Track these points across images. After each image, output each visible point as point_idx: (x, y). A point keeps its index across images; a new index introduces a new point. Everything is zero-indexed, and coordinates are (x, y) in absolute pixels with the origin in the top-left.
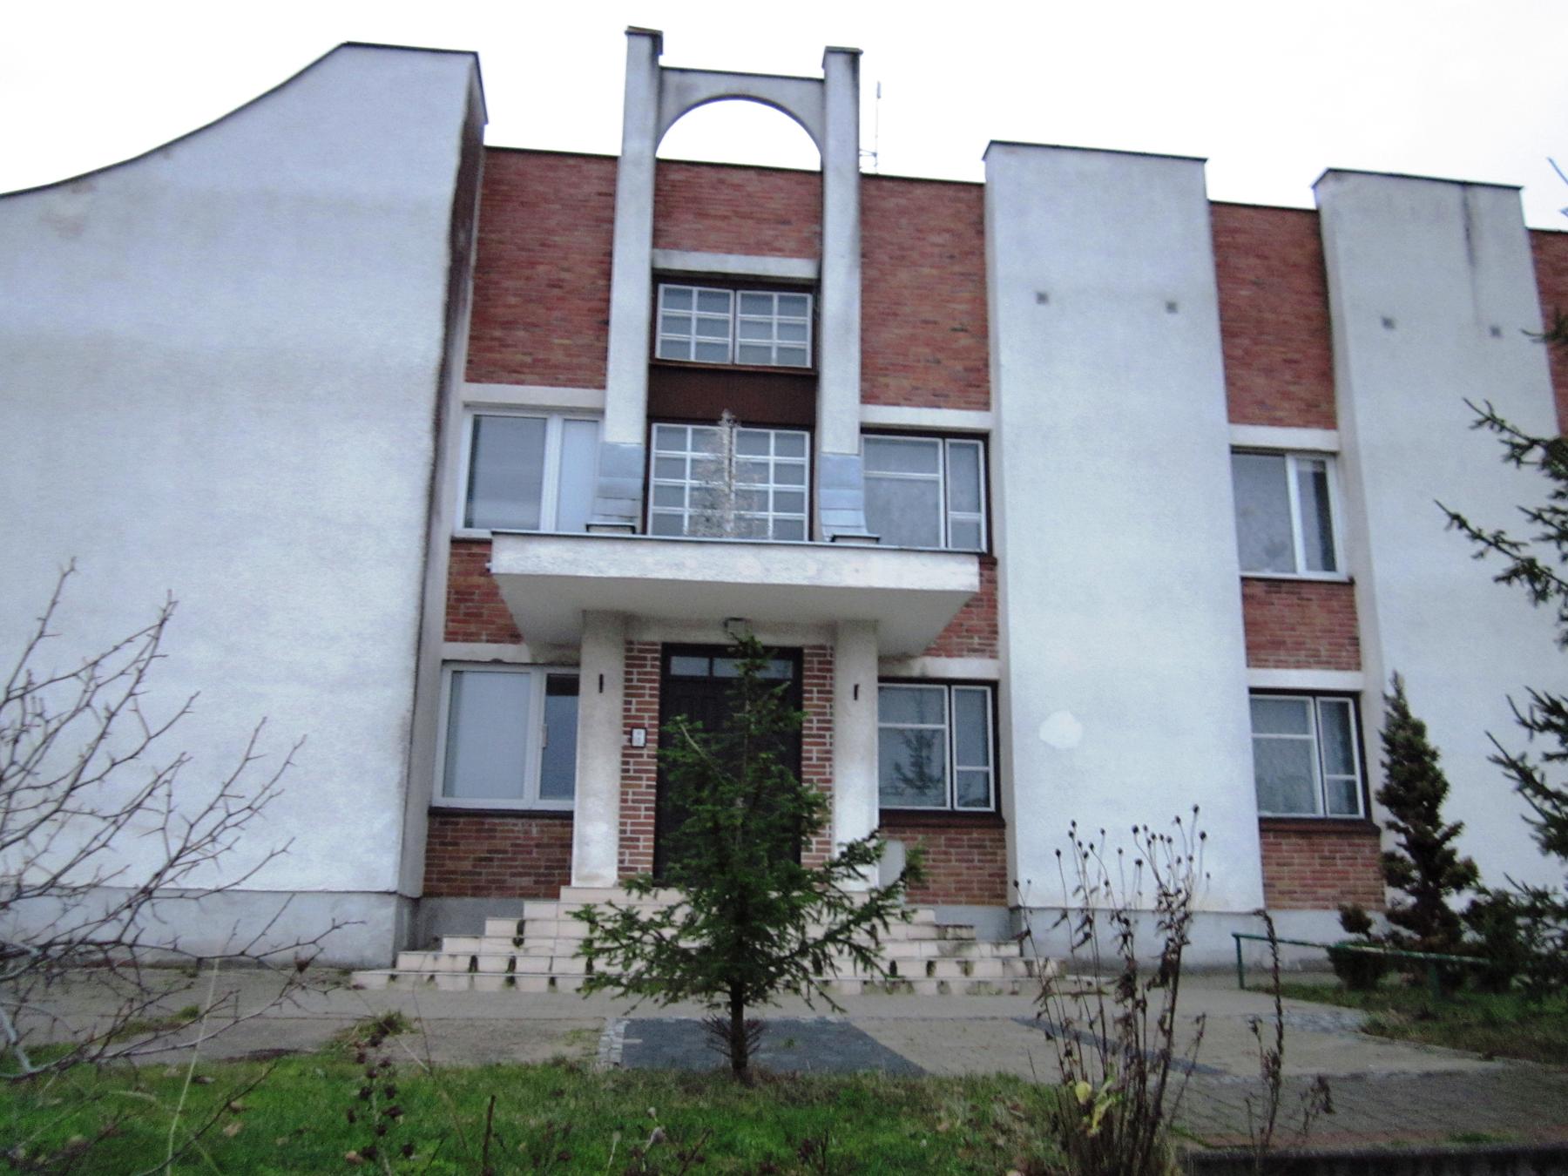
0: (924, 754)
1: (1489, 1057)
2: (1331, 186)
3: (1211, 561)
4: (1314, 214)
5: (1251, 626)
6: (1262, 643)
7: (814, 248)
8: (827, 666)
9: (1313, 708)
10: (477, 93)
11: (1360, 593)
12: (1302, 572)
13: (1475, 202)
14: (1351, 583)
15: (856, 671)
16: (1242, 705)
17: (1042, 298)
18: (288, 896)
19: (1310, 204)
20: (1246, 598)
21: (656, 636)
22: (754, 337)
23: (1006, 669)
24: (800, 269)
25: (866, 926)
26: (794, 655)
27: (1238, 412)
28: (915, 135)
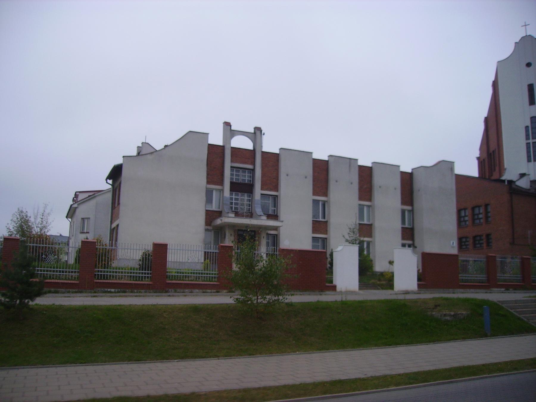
0: (271, 248)
2: (330, 157)
3: (309, 218)
4: (327, 161)
5: (313, 227)
6: (314, 231)
7: (254, 163)
8: (259, 234)
9: (320, 240)
10: (493, 146)
11: (328, 223)
12: (321, 219)
13: (352, 161)
14: (327, 222)
15: (264, 235)
16: (310, 240)
17: (287, 175)
18: (154, 150)
19: (278, 153)
20: (313, 223)
21: (237, 228)
22: (245, 178)
23: (279, 233)
24: (251, 167)
26: (254, 231)
27: (314, 194)
28: (270, 145)
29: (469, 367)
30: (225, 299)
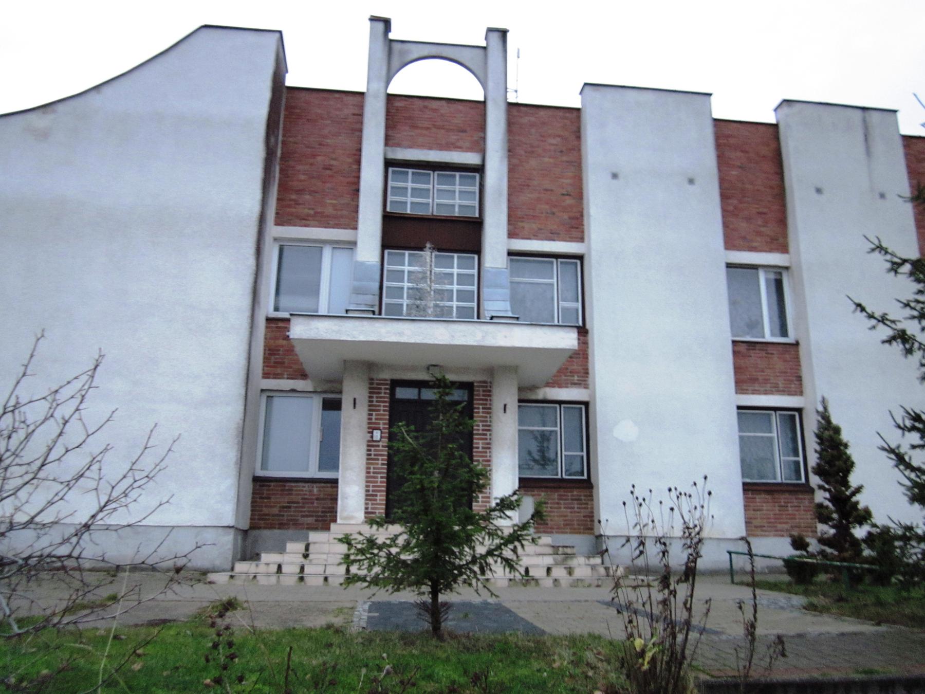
0: (545, 445)
2: (785, 109)
3: (715, 331)
4: (775, 127)
5: (738, 369)
6: (744, 379)
7: (480, 146)
8: (488, 393)
9: (775, 418)
11: (802, 350)
12: (768, 338)
13: (870, 119)
14: (797, 344)
15: (505, 396)
16: (732, 416)
17: (615, 176)
20: (735, 353)
21: (387, 375)
22: (445, 199)
23: (593, 395)
24: (472, 158)
26: (468, 387)
27: (730, 243)
28: (540, 80)
29: (428, 162)
30: (658, 670)
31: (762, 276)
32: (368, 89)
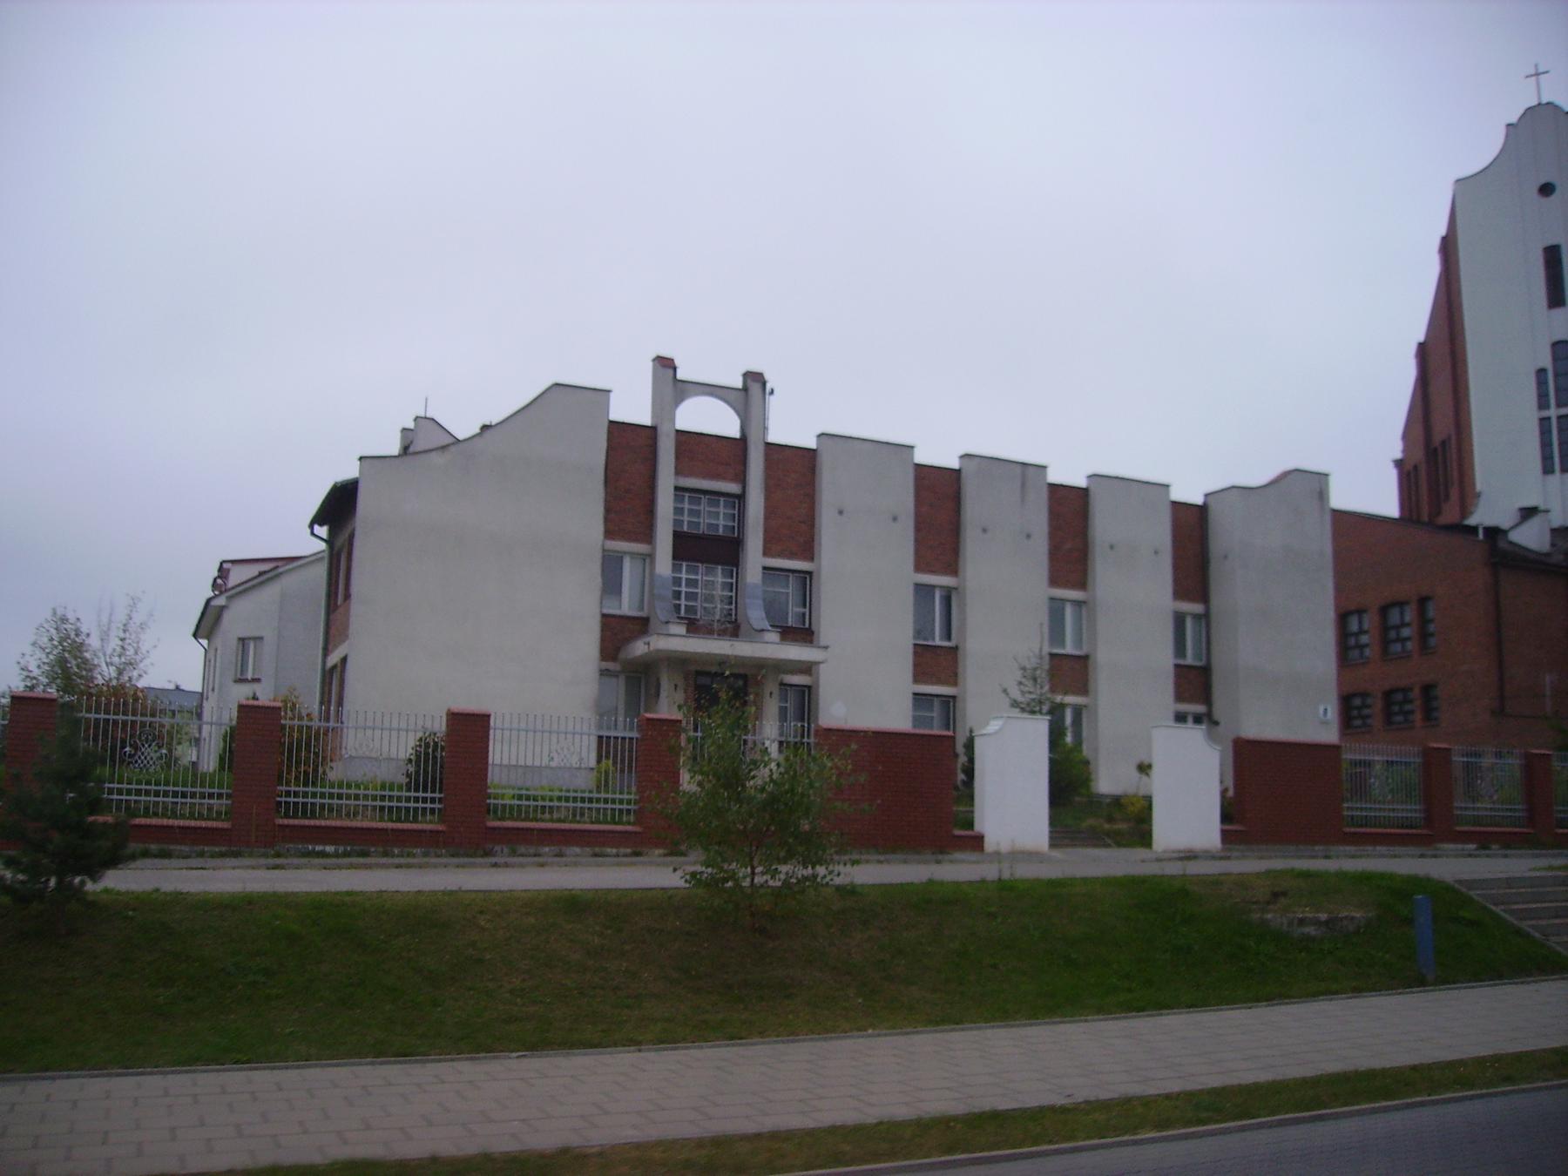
0: (793, 724)
1: (1447, 497)
2: (966, 460)
3: (903, 639)
4: (958, 472)
5: (916, 665)
6: (920, 674)
7: (742, 478)
8: (759, 684)
9: (936, 702)
11: (960, 652)
12: (938, 642)
13: (1028, 472)
14: (956, 648)
15: (771, 687)
16: (908, 702)
17: (841, 512)
20: (915, 653)
21: (693, 668)
22: (717, 520)
23: (817, 682)
24: (733, 488)
25: (553, 764)
26: (744, 677)
27: (919, 568)
28: (790, 425)
31: (936, 702)
32: (989, 855)
